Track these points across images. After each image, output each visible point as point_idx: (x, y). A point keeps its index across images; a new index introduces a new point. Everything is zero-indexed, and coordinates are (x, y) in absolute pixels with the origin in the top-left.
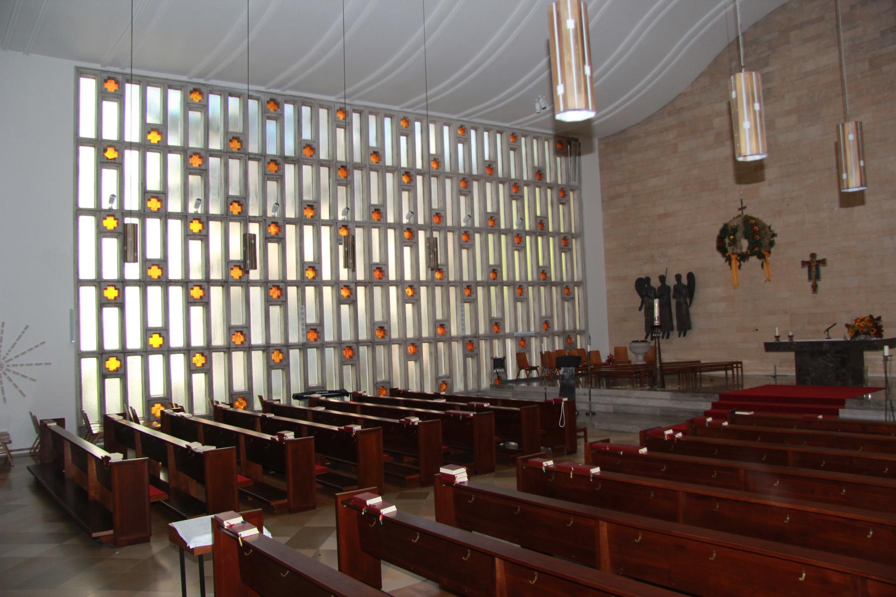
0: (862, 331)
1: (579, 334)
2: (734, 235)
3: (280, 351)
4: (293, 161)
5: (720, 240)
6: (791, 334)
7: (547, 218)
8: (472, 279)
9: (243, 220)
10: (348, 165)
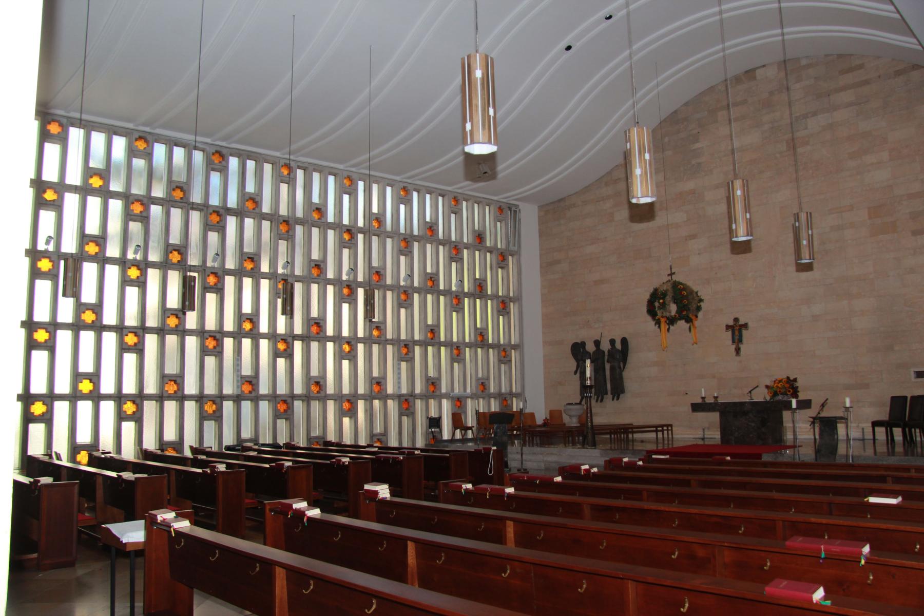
0: (780, 391)
1: (516, 397)
2: (663, 299)
3: (214, 402)
4: (235, 213)
5: (651, 303)
6: (716, 395)
7: (486, 280)
8: (409, 338)
9: (183, 269)
10: (290, 220)
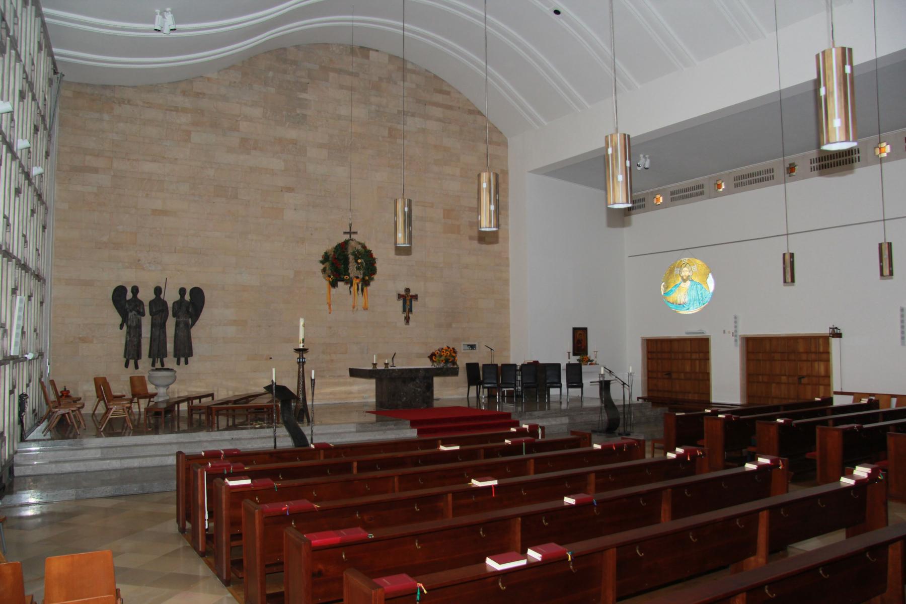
6: (386, 362)
